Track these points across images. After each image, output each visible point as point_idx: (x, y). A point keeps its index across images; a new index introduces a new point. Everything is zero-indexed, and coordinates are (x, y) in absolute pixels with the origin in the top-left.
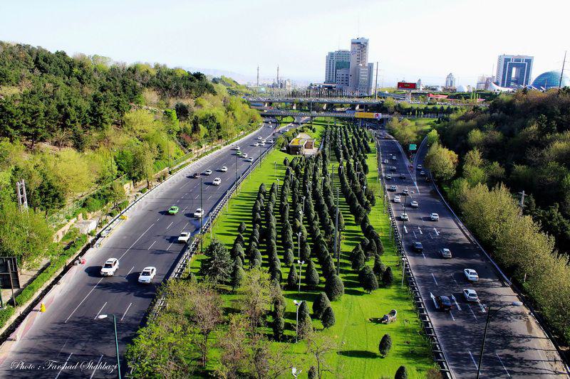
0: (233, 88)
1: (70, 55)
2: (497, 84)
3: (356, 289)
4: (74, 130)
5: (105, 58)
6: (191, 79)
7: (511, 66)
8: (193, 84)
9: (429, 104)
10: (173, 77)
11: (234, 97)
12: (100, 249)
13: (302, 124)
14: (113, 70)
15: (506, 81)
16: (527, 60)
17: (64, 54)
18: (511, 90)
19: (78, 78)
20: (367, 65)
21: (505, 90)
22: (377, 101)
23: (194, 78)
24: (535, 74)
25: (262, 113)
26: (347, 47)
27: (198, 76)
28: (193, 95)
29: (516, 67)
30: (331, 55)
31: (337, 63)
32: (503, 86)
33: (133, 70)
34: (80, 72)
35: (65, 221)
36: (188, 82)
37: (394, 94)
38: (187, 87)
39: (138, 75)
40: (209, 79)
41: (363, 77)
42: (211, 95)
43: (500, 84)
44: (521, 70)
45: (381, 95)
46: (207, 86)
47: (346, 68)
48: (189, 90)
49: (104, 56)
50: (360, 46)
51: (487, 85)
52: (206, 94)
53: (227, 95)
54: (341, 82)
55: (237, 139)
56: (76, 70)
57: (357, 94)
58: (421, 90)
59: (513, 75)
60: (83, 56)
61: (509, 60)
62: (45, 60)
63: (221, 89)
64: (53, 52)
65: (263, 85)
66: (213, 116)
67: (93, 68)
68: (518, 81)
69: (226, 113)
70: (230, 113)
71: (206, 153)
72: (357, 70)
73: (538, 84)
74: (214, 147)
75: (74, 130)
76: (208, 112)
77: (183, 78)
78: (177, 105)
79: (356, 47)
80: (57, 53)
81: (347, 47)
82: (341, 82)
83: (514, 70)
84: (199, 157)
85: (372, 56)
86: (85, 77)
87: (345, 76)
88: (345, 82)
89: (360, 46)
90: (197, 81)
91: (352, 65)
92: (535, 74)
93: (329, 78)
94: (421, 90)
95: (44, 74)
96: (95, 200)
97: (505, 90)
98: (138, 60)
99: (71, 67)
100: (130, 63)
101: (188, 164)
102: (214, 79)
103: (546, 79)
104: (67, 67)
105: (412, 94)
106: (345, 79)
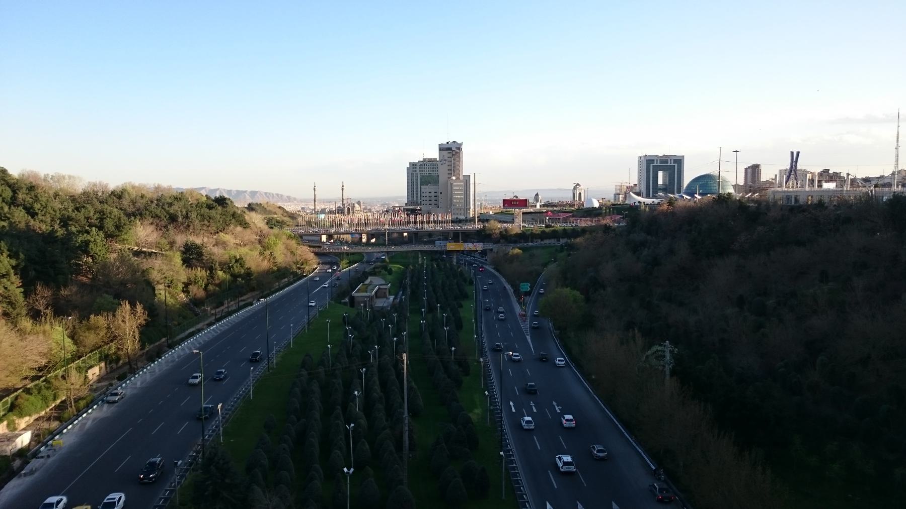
0: (278, 216)
2: (638, 194)
3: (529, 340)
5: (74, 177)
6: (210, 207)
7: (656, 169)
8: (213, 212)
9: (547, 227)
12: (28, 479)
13: (375, 262)
15: (651, 188)
16: (675, 161)
18: (656, 201)
19: (25, 208)
21: (649, 201)
22: (478, 226)
23: (215, 204)
25: (317, 250)
26: (435, 154)
27: (221, 201)
28: (213, 229)
29: (662, 169)
30: (413, 165)
32: (648, 196)
33: (118, 195)
34: (29, 199)
39: (126, 202)
40: (240, 204)
41: (458, 196)
42: (239, 229)
43: (644, 195)
45: (483, 219)
46: (234, 215)
47: (434, 177)
48: (206, 222)
49: (72, 174)
50: (451, 151)
52: (232, 227)
53: (265, 228)
55: (480, 336)
56: (21, 196)
57: (449, 217)
58: (538, 207)
59: (660, 182)
60: (36, 176)
61: (653, 161)
63: (257, 220)
66: (241, 259)
68: (667, 189)
70: (267, 253)
71: (230, 314)
72: (449, 186)
74: (242, 304)
76: (233, 253)
77: (199, 205)
78: (186, 245)
79: (445, 153)
81: (435, 154)
82: (428, 199)
84: (218, 320)
85: (468, 165)
86: (37, 206)
87: (433, 194)
88: (433, 202)
89: (451, 151)
90: (220, 208)
91: (442, 179)
94: (538, 207)
96: (32, 398)
97: (649, 201)
99: (14, 192)
101: (199, 331)
102: (250, 205)
103: (705, 182)
105: (523, 213)
106: (433, 198)
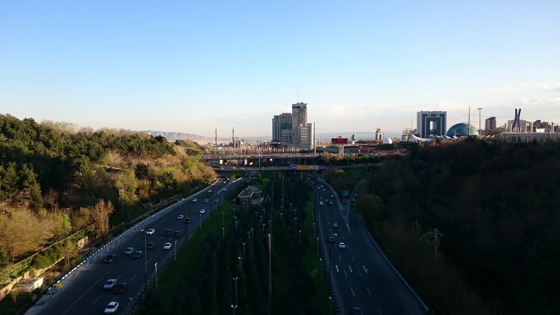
0: (194, 148)
1: (38, 121)
2: (417, 136)
3: (348, 227)
4: (32, 190)
5: (73, 124)
6: (153, 142)
7: (429, 120)
8: (155, 145)
10: (136, 140)
11: (192, 157)
12: (41, 307)
14: (79, 134)
15: (425, 131)
16: (441, 115)
17: (32, 121)
18: (429, 140)
20: (306, 125)
21: (424, 140)
22: (316, 155)
24: (449, 124)
25: (217, 169)
26: (290, 110)
28: (154, 155)
29: (432, 120)
30: (276, 117)
31: (282, 124)
32: (423, 137)
33: (99, 135)
35: (9, 280)
36: (150, 145)
37: (331, 149)
38: (148, 149)
39: (103, 139)
40: (171, 141)
41: (304, 136)
42: (170, 156)
43: (421, 136)
44: (437, 123)
45: (320, 150)
46: (167, 147)
47: (289, 125)
48: (150, 151)
49: (72, 122)
50: (300, 109)
51: (409, 136)
52: (166, 154)
53: (185, 155)
54: (285, 140)
60: (51, 123)
62: (13, 126)
64: (21, 119)
65: (221, 145)
67: (60, 133)
69: (183, 171)
70: (187, 170)
71: (164, 207)
72: (298, 130)
73: (451, 134)
74: (171, 201)
75: (32, 190)
77: (146, 141)
80: (26, 119)
81: (290, 110)
82: (285, 140)
83: (431, 123)
85: (310, 117)
87: (288, 135)
88: (288, 140)
89: (300, 109)
90: (159, 143)
91: (294, 126)
92: (449, 124)
93: (276, 137)
95: (10, 140)
96: (44, 258)
97: (424, 140)
98: (104, 126)
99: (38, 133)
100: (96, 128)
101: (145, 218)
102: (177, 141)
103: (460, 128)
104: (34, 133)
106: (289, 138)
